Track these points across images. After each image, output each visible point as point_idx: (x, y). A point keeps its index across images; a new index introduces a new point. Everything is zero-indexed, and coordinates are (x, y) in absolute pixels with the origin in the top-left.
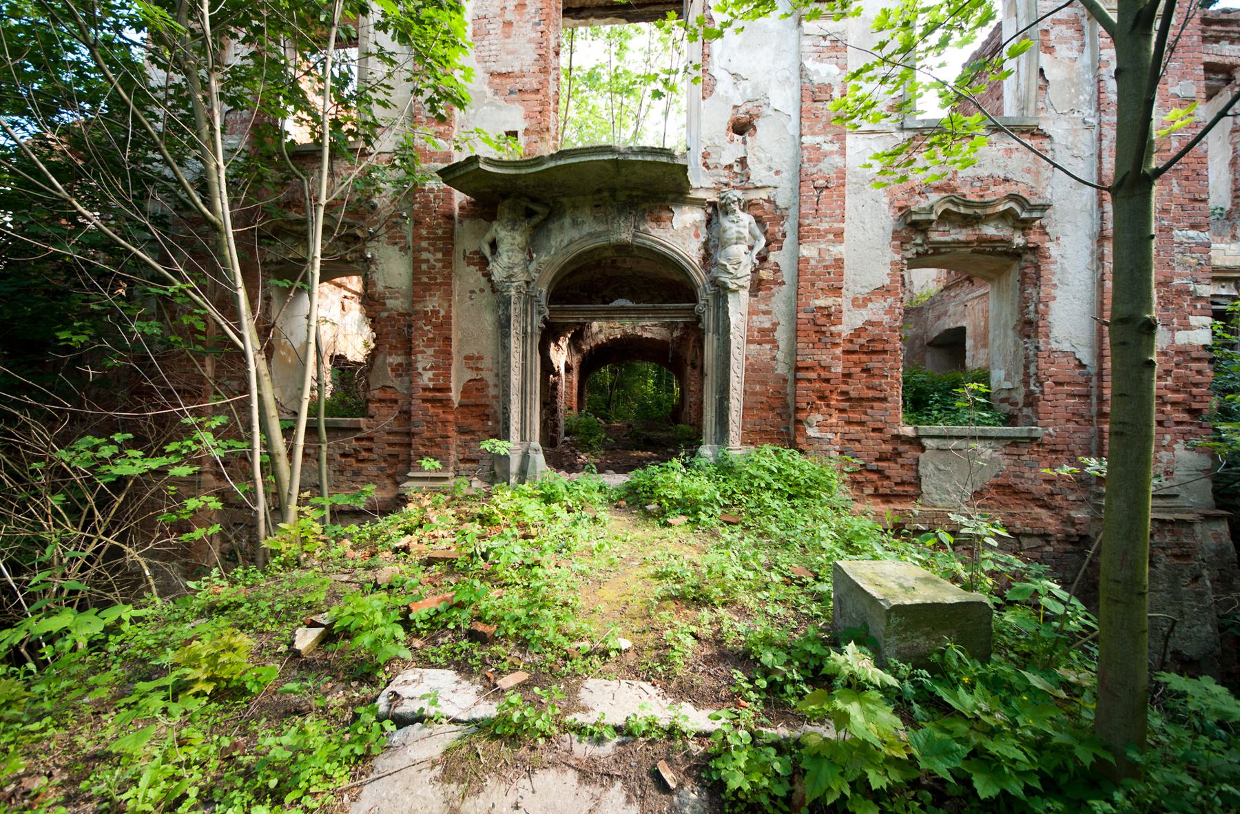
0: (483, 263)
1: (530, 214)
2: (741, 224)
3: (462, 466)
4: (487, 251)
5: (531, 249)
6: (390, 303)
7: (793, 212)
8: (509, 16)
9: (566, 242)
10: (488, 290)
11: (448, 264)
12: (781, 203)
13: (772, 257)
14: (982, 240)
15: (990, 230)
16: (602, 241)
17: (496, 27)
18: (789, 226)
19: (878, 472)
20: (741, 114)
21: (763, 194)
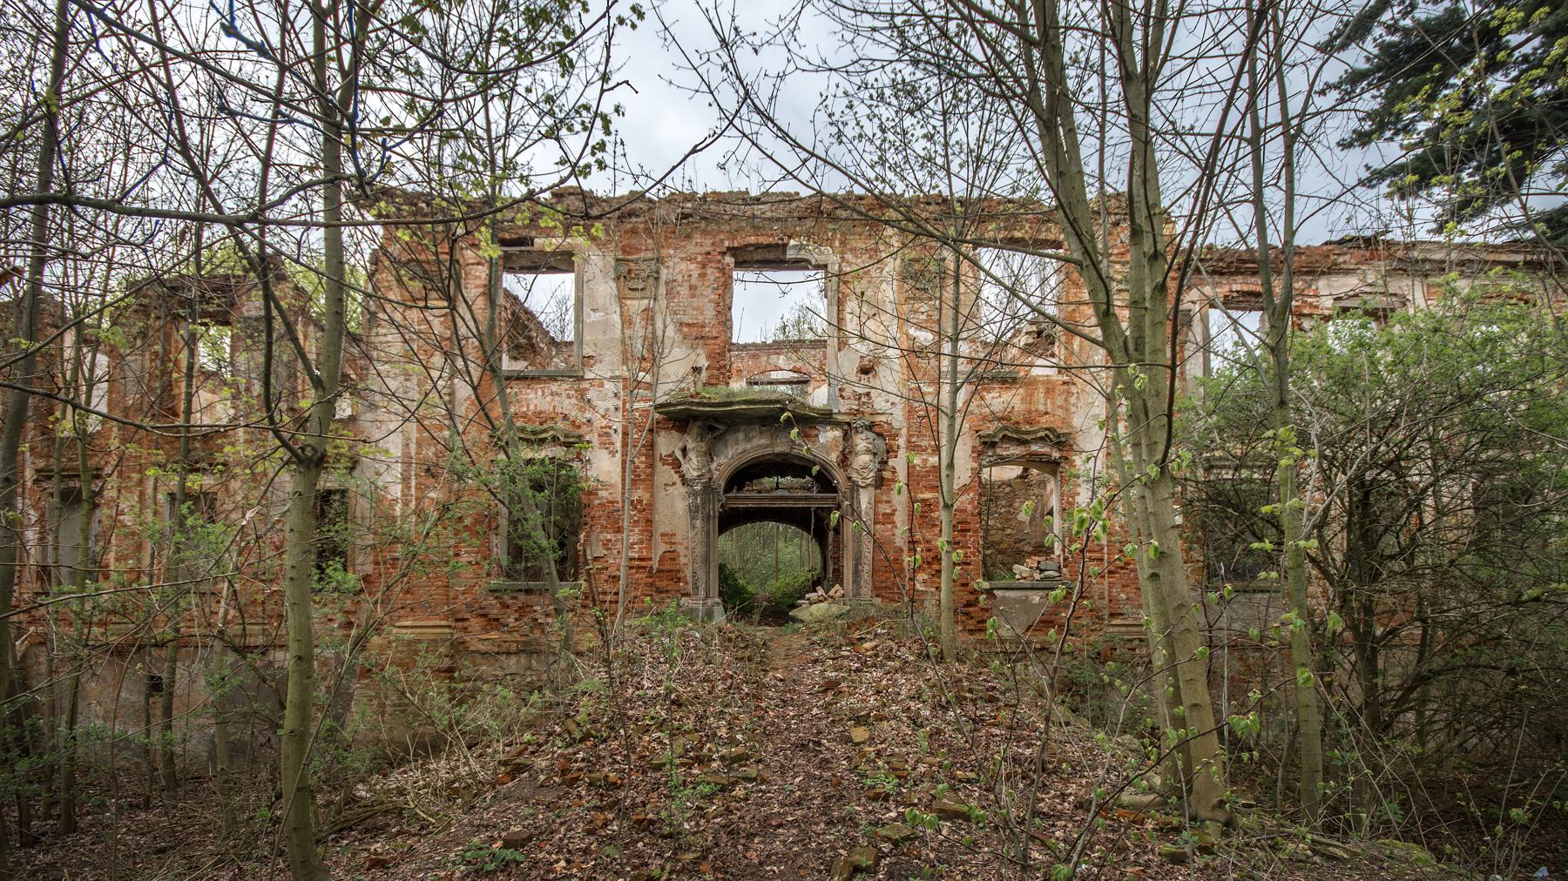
0: (676, 465)
1: (711, 429)
2: (861, 442)
3: (667, 443)
4: (679, 455)
5: (710, 455)
6: (601, 493)
7: (904, 431)
8: (693, 282)
9: (480, 304)
10: (679, 483)
11: (652, 466)
12: (896, 425)
13: (891, 462)
14: (1031, 454)
15: (1034, 448)
16: (768, 451)
17: (684, 290)
18: (902, 441)
19: (966, 614)
20: (866, 362)
21: (883, 418)
